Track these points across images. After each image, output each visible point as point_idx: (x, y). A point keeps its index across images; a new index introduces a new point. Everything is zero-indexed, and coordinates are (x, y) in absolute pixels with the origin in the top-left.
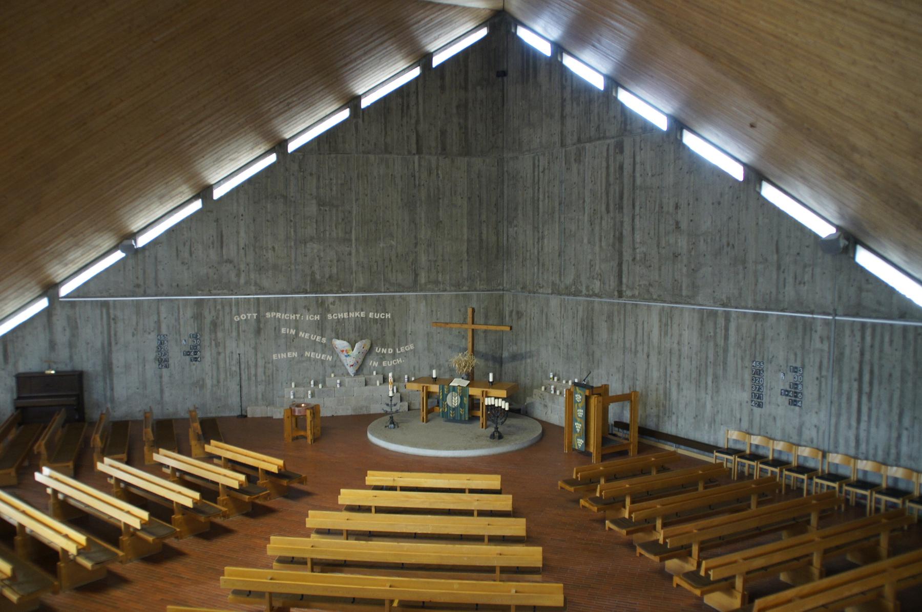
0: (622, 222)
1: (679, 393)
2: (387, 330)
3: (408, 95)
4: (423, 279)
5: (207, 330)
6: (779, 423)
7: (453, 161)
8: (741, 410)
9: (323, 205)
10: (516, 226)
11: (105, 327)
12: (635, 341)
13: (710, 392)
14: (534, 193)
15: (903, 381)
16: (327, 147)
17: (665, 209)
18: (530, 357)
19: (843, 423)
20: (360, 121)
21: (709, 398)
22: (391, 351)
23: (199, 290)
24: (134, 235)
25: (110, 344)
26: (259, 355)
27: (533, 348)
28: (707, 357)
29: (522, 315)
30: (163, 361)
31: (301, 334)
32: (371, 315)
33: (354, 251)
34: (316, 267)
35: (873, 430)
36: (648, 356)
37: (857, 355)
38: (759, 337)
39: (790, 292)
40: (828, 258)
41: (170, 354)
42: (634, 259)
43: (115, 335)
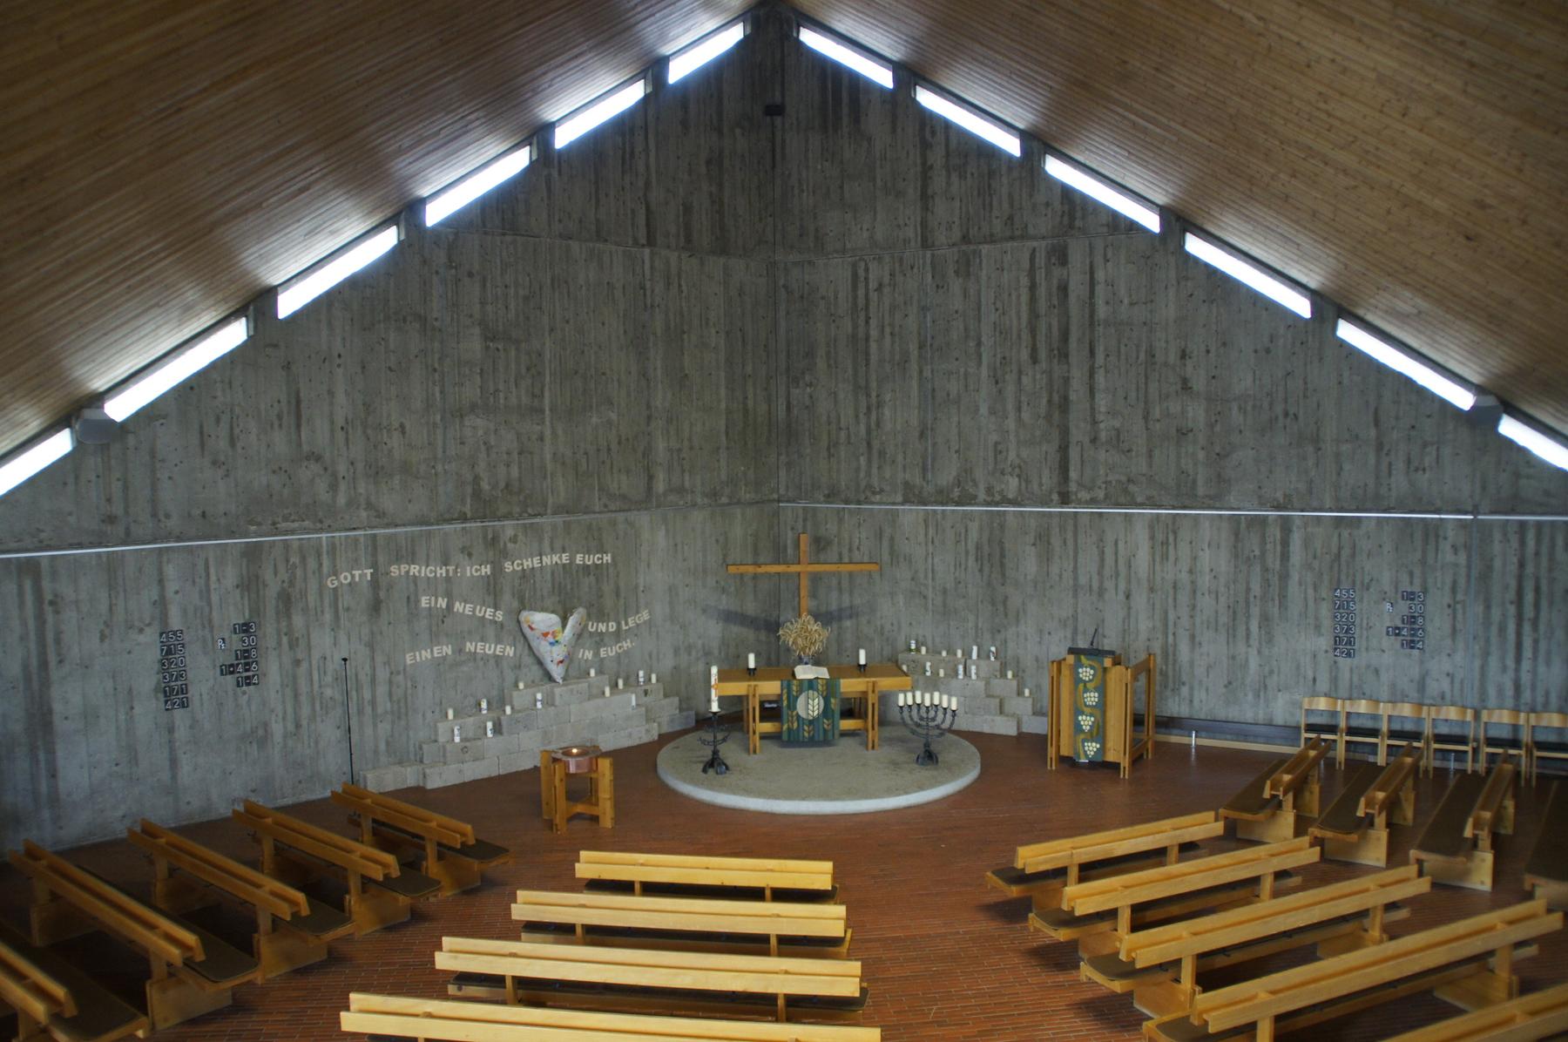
0: (1067, 380)
1: (1192, 649)
4: (660, 486)
5: (270, 611)
6: (1384, 677)
7: (702, 264)
9: (493, 339)
10: (811, 385)
11: (31, 624)
12: (1100, 574)
13: (1254, 642)
14: (855, 326)
17: (1160, 358)
18: (851, 617)
19: (1494, 662)
20: (555, 173)
21: (1253, 652)
22: (612, 627)
23: (251, 522)
24: (99, 398)
25: (44, 665)
26: (379, 659)
27: (857, 601)
28: (1248, 590)
29: (829, 543)
30: (174, 693)
31: (458, 607)
32: (579, 559)
33: (548, 432)
34: (482, 465)
35: (1542, 669)
36: (1128, 597)
37: (1513, 568)
38: (1346, 553)
39: (1399, 482)
41: (191, 675)
42: (1094, 440)
43: (58, 641)
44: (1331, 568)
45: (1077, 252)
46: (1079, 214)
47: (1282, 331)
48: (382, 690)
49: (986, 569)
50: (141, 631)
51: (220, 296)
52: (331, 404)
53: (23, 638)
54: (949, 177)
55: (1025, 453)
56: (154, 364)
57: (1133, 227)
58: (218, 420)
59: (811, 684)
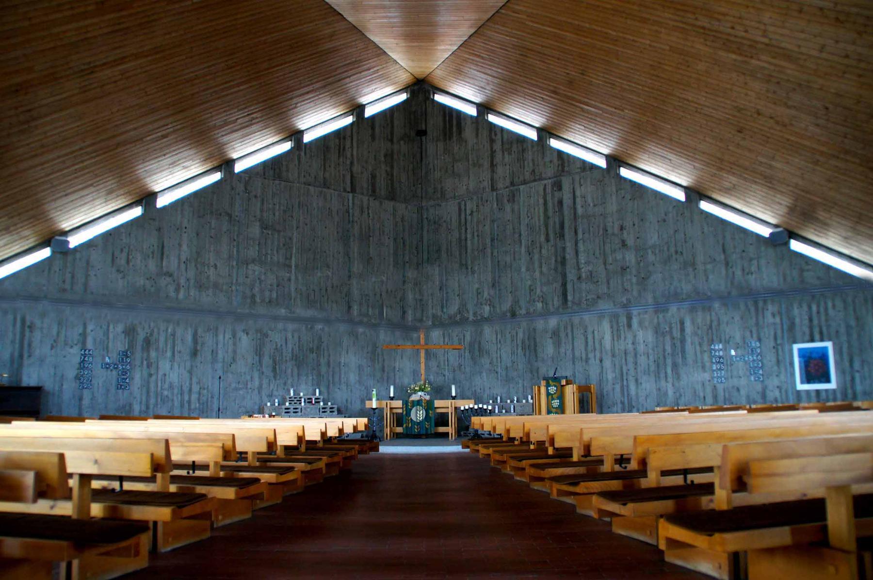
0: (564, 249)
1: (637, 387)
2: (322, 360)
3: (344, 138)
5: (139, 348)
7: (381, 203)
8: (704, 390)
11: (18, 337)
12: (586, 350)
13: (670, 380)
14: (460, 234)
15: (849, 334)
16: (271, 172)
17: (610, 231)
20: (303, 154)
21: (670, 385)
24: (65, 233)
25: (21, 356)
26: (194, 380)
28: (664, 350)
33: (293, 278)
34: (256, 290)
36: (601, 361)
37: (806, 322)
40: (771, 251)
42: (579, 278)
43: (30, 345)
44: (708, 334)
45: (566, 183)
46: (566, 165)
47: (670, 209)
48: (194, 397)
49: (527, 353)
50: (72, 347)
51: (126, 189)
52: (180, 250)
53: (13, 342)
54: (503, 154)
55: (545, 289)
56: (91, 218)
57: (593, 167)
58: (122, 250)
59: (419, 403)
